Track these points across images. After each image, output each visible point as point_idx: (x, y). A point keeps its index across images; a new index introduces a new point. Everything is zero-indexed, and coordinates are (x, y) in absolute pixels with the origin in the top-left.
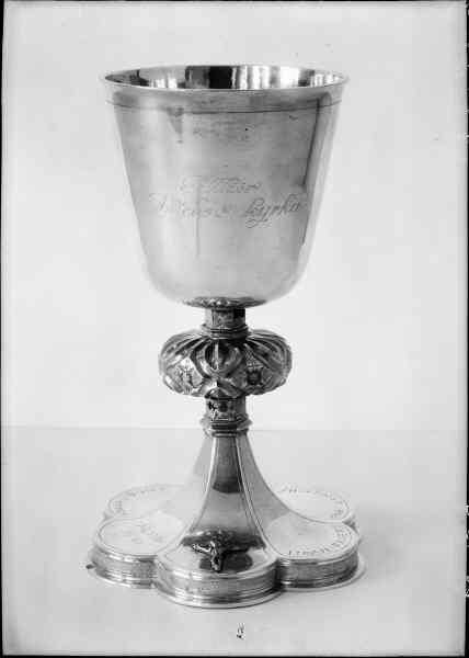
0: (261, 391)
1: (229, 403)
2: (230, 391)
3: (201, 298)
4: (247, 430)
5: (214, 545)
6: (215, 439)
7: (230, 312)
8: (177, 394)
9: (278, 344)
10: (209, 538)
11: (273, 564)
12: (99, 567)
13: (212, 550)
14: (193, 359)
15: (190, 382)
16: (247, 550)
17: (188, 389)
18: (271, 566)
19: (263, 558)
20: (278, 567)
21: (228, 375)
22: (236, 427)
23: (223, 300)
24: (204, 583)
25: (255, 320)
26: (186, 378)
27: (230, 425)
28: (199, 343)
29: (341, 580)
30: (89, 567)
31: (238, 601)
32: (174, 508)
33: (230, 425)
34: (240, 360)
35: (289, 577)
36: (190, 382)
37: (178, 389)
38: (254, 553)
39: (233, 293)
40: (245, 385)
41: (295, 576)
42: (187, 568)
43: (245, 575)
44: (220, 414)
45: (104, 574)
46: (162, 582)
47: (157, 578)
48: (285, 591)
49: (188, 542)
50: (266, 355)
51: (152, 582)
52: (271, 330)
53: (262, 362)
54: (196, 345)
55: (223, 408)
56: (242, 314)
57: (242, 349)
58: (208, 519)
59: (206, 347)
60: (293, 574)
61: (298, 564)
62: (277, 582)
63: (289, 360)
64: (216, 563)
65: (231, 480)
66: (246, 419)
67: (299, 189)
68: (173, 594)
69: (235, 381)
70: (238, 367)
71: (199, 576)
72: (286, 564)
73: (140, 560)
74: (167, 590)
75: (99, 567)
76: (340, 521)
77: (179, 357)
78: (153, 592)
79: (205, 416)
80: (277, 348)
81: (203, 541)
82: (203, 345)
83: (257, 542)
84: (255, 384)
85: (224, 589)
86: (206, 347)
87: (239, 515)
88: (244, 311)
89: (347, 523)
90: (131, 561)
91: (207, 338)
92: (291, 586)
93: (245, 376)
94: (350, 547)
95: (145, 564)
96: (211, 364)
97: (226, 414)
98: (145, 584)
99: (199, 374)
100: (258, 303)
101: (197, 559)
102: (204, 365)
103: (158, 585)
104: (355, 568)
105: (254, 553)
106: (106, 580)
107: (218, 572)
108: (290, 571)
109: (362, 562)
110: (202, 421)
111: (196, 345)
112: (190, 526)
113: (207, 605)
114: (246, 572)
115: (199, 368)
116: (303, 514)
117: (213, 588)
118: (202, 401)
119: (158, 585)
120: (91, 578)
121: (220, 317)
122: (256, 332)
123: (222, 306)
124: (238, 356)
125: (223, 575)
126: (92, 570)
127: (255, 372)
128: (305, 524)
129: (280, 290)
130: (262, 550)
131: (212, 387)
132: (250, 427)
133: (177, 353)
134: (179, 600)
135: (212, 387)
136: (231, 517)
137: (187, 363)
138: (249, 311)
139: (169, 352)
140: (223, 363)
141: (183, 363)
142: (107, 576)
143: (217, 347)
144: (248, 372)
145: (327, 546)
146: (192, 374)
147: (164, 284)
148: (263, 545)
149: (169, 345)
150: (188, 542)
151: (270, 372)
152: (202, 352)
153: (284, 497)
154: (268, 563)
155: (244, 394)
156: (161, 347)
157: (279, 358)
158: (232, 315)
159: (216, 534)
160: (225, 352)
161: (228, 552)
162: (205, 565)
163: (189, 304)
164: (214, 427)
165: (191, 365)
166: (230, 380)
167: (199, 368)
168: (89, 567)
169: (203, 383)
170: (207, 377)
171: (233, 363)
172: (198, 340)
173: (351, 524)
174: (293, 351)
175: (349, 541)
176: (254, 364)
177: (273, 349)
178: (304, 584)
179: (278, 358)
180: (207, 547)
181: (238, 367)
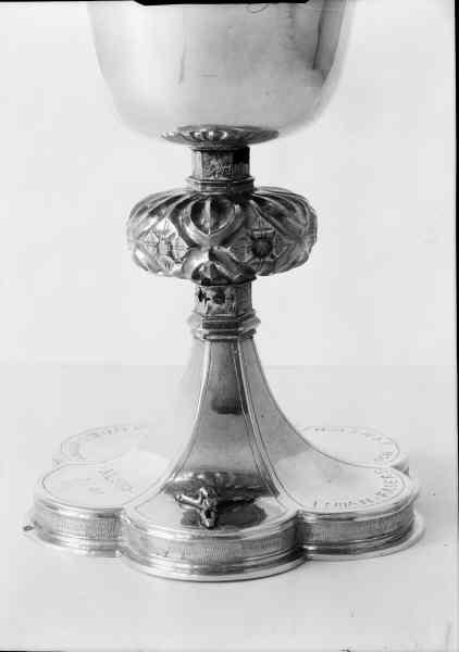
0: (271, 269)
1: (228, 291)
2: (227, 268)
3: (186, 129)
4: (253, 331)
5: (205, 493)
6: (208, 343)
7: (227, 152)
8: (153, 275)
9: (296, 202)
10: (203, 484)
11: (292, 519)
12: (44, 529)
13: (203, 501)
14: (174, 218)
15: (170, 254)
16: (252, 500)
17: (168, 265)
18: (287, 522)
19: (278, 509)
20: (299, 524)
21: (224, 243)
22: (237, 325)
23: (218, 130)
24: (191, 544)
25: (267, 168)
26: (164, 248)
27: (230, 324)
28: (181, 200)
29: (390, 544)
30: (27, 529)
31: (241, 570)
32: (155, 438)
33: (230, 324)
34: (240, 221)
35: (315, 539)
36: (170, 254)
37: (153, 268)
38: (264, 502)
39: (231, 114)
40: (248, 257)
41: (322, 538)
42: (166, 527)
43: (252, 533)
44: (215, 306)
45: (50, 537)
46: (130, 547)
47: (125, 541)
48: (308, 560)
49: (170, 489)
50: (279, 216)
51: (117, 547)
52: (285, 187)
53: (274, 225)
54: (177, 203)
55: (219, 298)
56: (242, 156)
57: (244, 206)
58: (198, 459)
59: (192, 203)
60: (321, 534)
61: (327, 519)
62: (297, 545)
63: (313, 228)
64: (208, 516)
65: (233, 399)
66: (252, 316)
67: (397, 461)
68: (148, 564)
69: (235, 250)
70: (238, 231)
71: (185, 534)
72: (310, 519)
73: (100, 516)
74: (141, 557)
75: (44, 529)
76: (387, 465)
77: (153, 220)
78: (118, 563)
79: (195, 311)
80: (298, 209)
81: (191, 489)
82: (187, 202)
83: (268, 489)
84: (265, 256)
85: (219, 553)
86: (192, 203)
87: (161, 226)
88: (249, 149)
89: (396, 467)
90: (87, 517)
91: (196, 194)
92: (318, 552)
93: (248, 243)
94: (403, 496)
95: (105, 521)
96: (200, 227)
97: (223, 307)
98: (108, 550)
99: (182, 242)
100: (265, 135)
101: (179, 513)
102: (191, 230)
103: (124, 551)
104: (410, 529)
105: (264, 502)
106: (49, 545)
107: (210, 528)
108: (315, 530)
109: (419, 520)
110: (190, 320)
111: (177, 203)
112: (174, 465)
113: (195, 577)
114: (255, 528)
115: (183, 234)
116: (334, 455)
117: (204, 552)
118: (192, 287)
119: (124, 551)
120: (32, 540)
121: (213, 162)
122: (265, 188)
123: (216, 139)
124: (237, 217)
125: (217, 533)
126: (30, 532)
127: (263, 238)
128: (336, 468)
129: (301, 117)
130: (273, 498)
131: (201, 260)
132: (258, 329)
133: (152, 214)
134: (158, 573)
135: (201, 260)
136: (240, 459)
137: (165, 224)
138: (256, 150)
139: (141, 213)
140: (217, 224)
141: (161, 226)
142: (54, 541)
143: (208, 204)
144: (252, 238)
145: (369, 496)
146: (173, 242)
147: (135, 116)
148: (275, 493)
149: (142, 203)
150: (170, 489)
151: (285, 240)
152: (189, 209)
153: (308, 436)
154: (286, 517)
155: (248, 276)
156: (129, 213)
157: (297, 221)
158: (230, 158)
159: (210, 475)
160: (219, 210)
161: (227, 502)
162: (192, 521)
163: (170, 138)
164: (207, 326)
165: (173, 229)
166: (228, 250)
167: (183, 234)
168: (27, 529)
169: (188, 255)
170: (194, 246)
171: (231, 226)
172: (179, 197)
173: (402, 468)
174: (318, 213)
175: (402, 488)
176: (261, 226)
177: (291, 208)
178: (337, 549)
179: (297, 220)
180: (196, 497)
181: (238, 231)
